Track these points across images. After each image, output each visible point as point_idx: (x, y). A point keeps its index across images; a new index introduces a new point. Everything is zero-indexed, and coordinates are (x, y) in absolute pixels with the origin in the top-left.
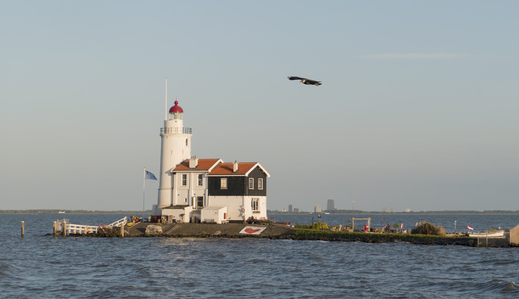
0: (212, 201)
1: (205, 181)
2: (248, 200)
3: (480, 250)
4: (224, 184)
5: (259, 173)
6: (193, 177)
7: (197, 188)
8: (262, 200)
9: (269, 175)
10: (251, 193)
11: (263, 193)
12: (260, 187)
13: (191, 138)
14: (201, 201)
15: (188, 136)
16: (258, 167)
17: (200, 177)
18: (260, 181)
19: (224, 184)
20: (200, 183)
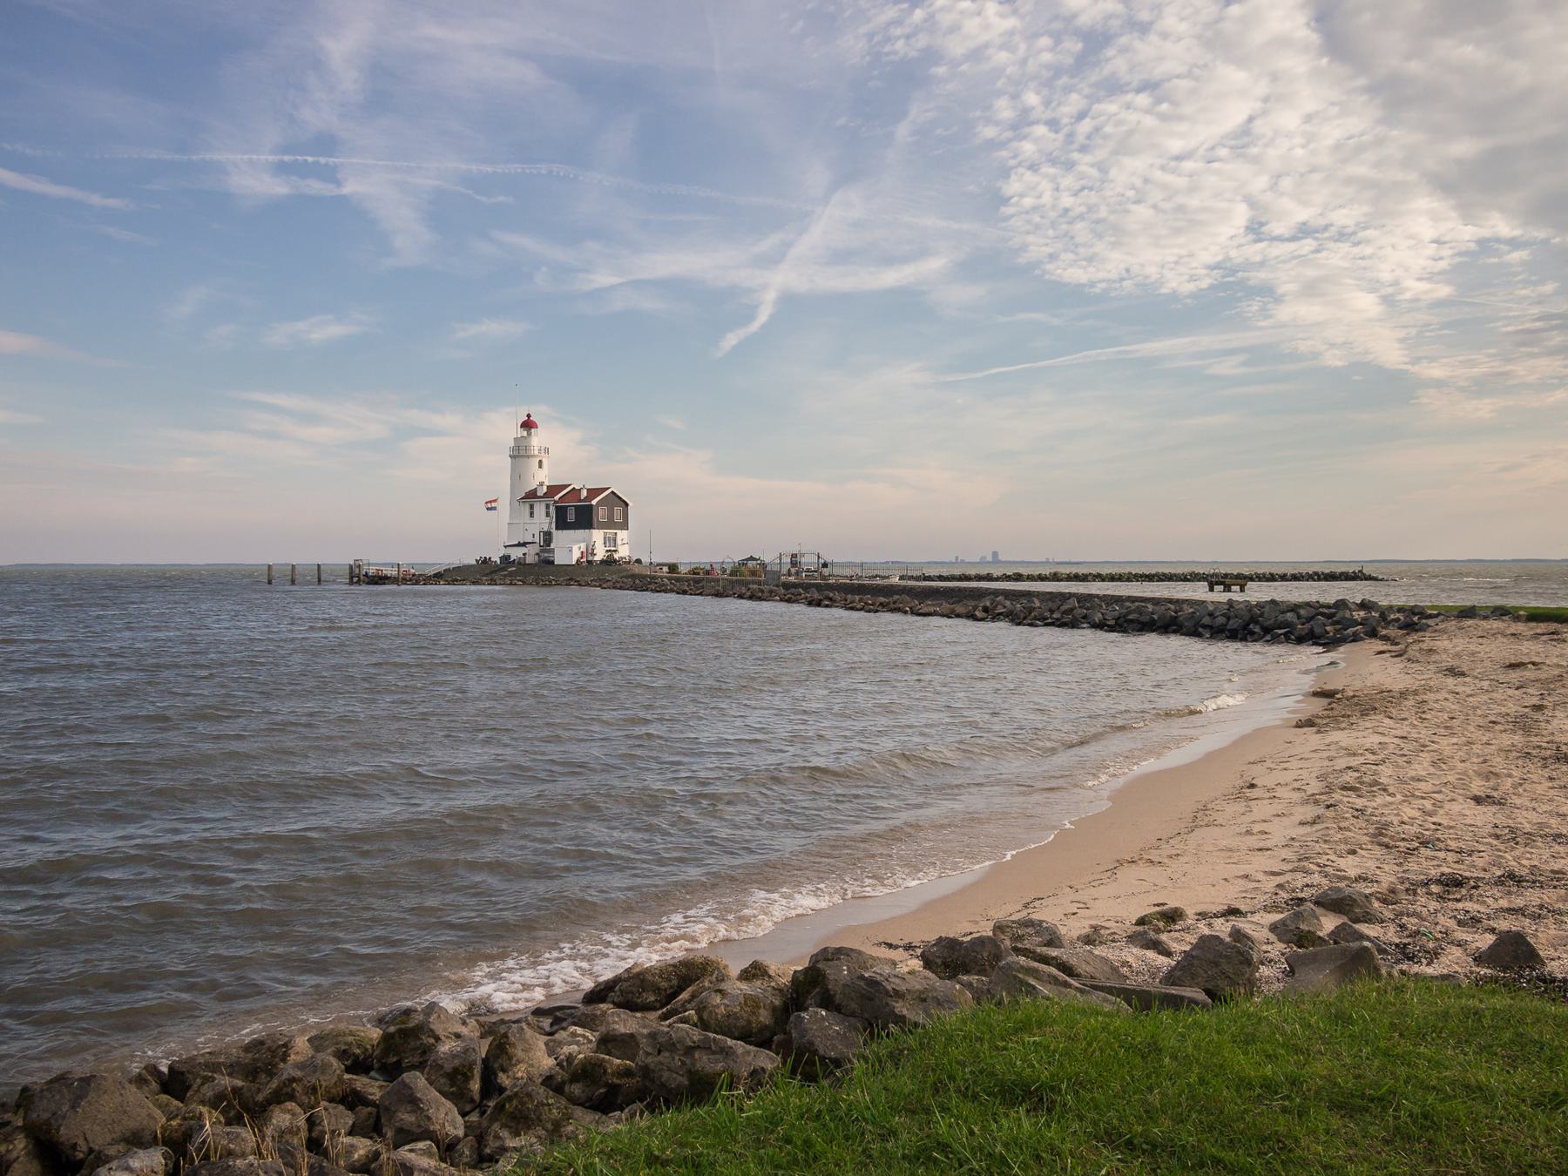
0: (561, 538)
1: (552, 509)
2: (597, 536)
3: (969, 631)
4: (571, 517)
5: (617, 501)
6: (540, 509)
7: (543, 519)
8: (622, 535)
10: (602, 526)
11: (624, 525)
12: (618, 519)
14: (548, 537)
17: (548, 507)
18: (618, 510)
19: (571, 517)
20: (548, 514)
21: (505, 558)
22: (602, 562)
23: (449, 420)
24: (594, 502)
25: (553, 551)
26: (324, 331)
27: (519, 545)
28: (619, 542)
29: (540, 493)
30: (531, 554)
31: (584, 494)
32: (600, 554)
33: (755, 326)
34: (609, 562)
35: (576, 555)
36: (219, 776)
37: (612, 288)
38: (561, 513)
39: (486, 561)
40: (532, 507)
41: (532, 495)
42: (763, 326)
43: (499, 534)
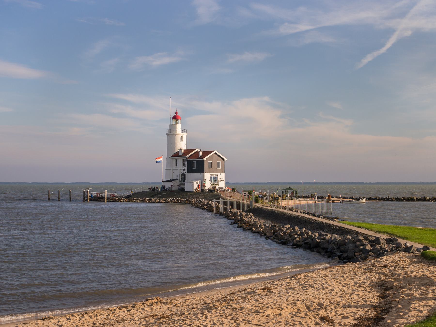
4: (194, 166)
6: (180, 162)
7: (181, 168)
9: (226, 159)
13: (187, 136)
15: (185, 135)
16: (215, 153)
17: (184, 161)
19: (194, 166)
21: (163, 188)
22: (209, 190)
23: (215, 106)
24: (205, 159)
25: (184, 184)
26: (160, 60)
27: (171, 181)
28: (219, 180)
29: (180, 154)
30: (175, 186)
31: (201, 154)
32: (208, 185)
33: (383, 50)
34: (211, 191)
35: (195, 186)
36: (404, 291)
37: (307, 31)
38: (190, 164)
39: (154, 189)
40: (176, 161)
41: (176, 155)
42: (388, 50)
43: (159, 172)
